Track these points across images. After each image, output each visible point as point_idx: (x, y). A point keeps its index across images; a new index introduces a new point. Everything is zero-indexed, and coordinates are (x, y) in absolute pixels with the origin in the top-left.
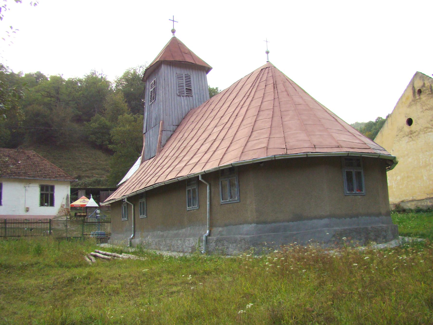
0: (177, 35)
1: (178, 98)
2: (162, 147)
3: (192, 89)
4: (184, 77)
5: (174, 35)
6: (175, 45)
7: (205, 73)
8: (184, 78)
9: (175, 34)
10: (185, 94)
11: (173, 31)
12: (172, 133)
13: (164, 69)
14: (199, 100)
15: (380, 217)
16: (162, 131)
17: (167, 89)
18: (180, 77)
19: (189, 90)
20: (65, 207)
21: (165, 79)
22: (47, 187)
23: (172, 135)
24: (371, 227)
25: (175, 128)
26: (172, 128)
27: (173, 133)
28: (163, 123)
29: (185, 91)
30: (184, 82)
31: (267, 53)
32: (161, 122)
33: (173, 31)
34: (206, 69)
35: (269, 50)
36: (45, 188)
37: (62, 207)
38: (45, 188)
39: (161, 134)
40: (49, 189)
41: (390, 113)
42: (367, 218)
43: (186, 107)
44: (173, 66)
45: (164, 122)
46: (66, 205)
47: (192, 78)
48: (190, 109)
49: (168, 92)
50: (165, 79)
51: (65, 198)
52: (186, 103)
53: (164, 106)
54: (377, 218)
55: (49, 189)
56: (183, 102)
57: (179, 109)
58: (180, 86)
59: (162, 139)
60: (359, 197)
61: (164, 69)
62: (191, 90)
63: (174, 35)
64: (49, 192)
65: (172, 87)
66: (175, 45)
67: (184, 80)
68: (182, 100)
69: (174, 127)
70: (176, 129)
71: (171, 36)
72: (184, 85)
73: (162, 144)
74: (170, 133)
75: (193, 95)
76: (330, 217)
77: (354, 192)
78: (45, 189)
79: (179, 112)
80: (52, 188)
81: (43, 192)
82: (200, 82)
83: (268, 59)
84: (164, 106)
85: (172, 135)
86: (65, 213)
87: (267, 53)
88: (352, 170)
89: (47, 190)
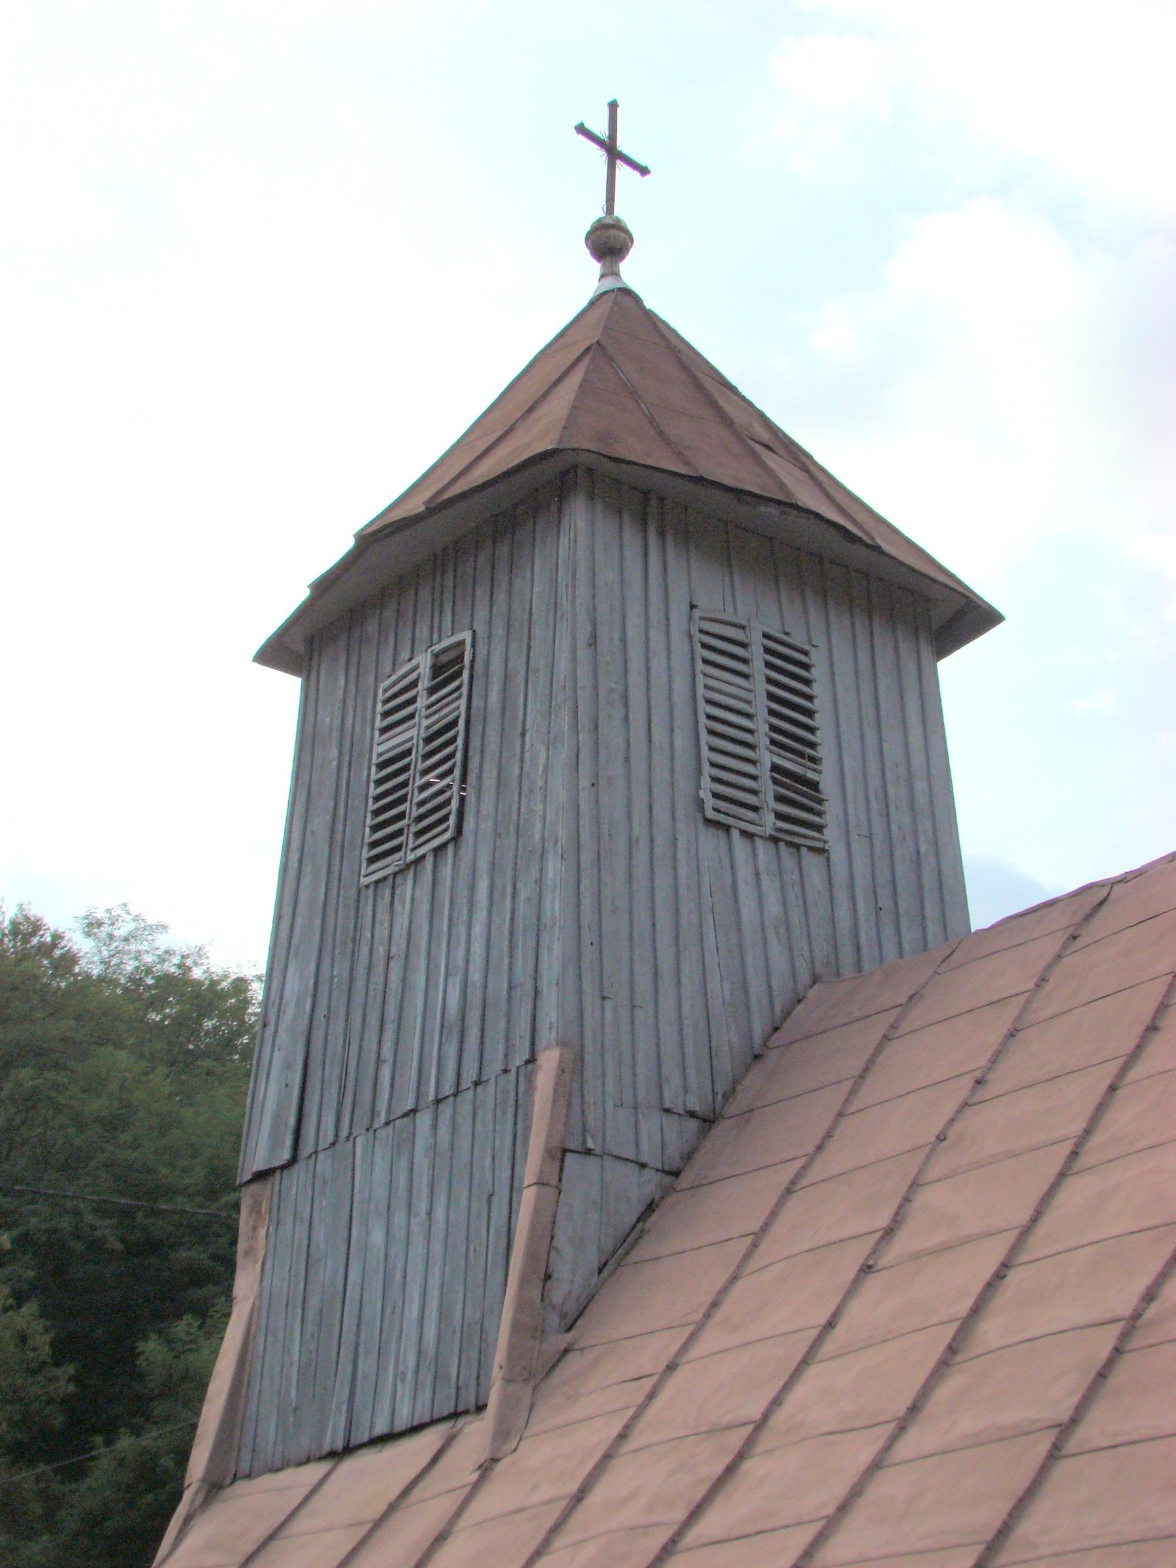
0: (633, 272)
1: (709, 841)
2: (554, 1320)
3: (827, 781)
4: (757, 657)
5: (610, 272)
6: (619, 344)
7: (926, 651)
8: (758, 668)
10: (769, 831)
11: (609, 243)
12: (650, 1183)
13: (583, 535)
14: (885, 902)
16: (559, 1154)
17: (613, 736)
18: (721, 650)
19: (800, 792)
21: (593, 642)
23: (650, 1208)
25: (678, 1134)
26: (657, 1137)
27: (667, 1191)
28: (574, 1071)
29: (768, 789)
30: (761, 705)
32: (549, 1060)
33: (609, 243)
34: (958, 616)
39: (553, 1184)
43: (777, 951)
44: (823, 594)
45: (581, 1059)
47: (818, 673)
48: (804, 977)
49: (619, 770)
50: (593, 642)
52: (773, 907)
53: (587, 902)
56: (746, 892)
57: (712, 959)
58: (726, 730)
59: (561, 1241)
61: (583, 535)
62: (814, 786)
63: (610, 272)
65: (659, 735)
66: (619, 344)
67: (761, 687)
68: (744, 872)
69: (670, 1122)
70: (688, 1157)
71: (584, 279)
72: (761, 725)
73: (559, 1293)
74: (636, 1188)
75: (832, 836)
76: (812, 957)
79: (713, 985)
82: (891, 730)
84: (587, 902)
85: (650, 1208)
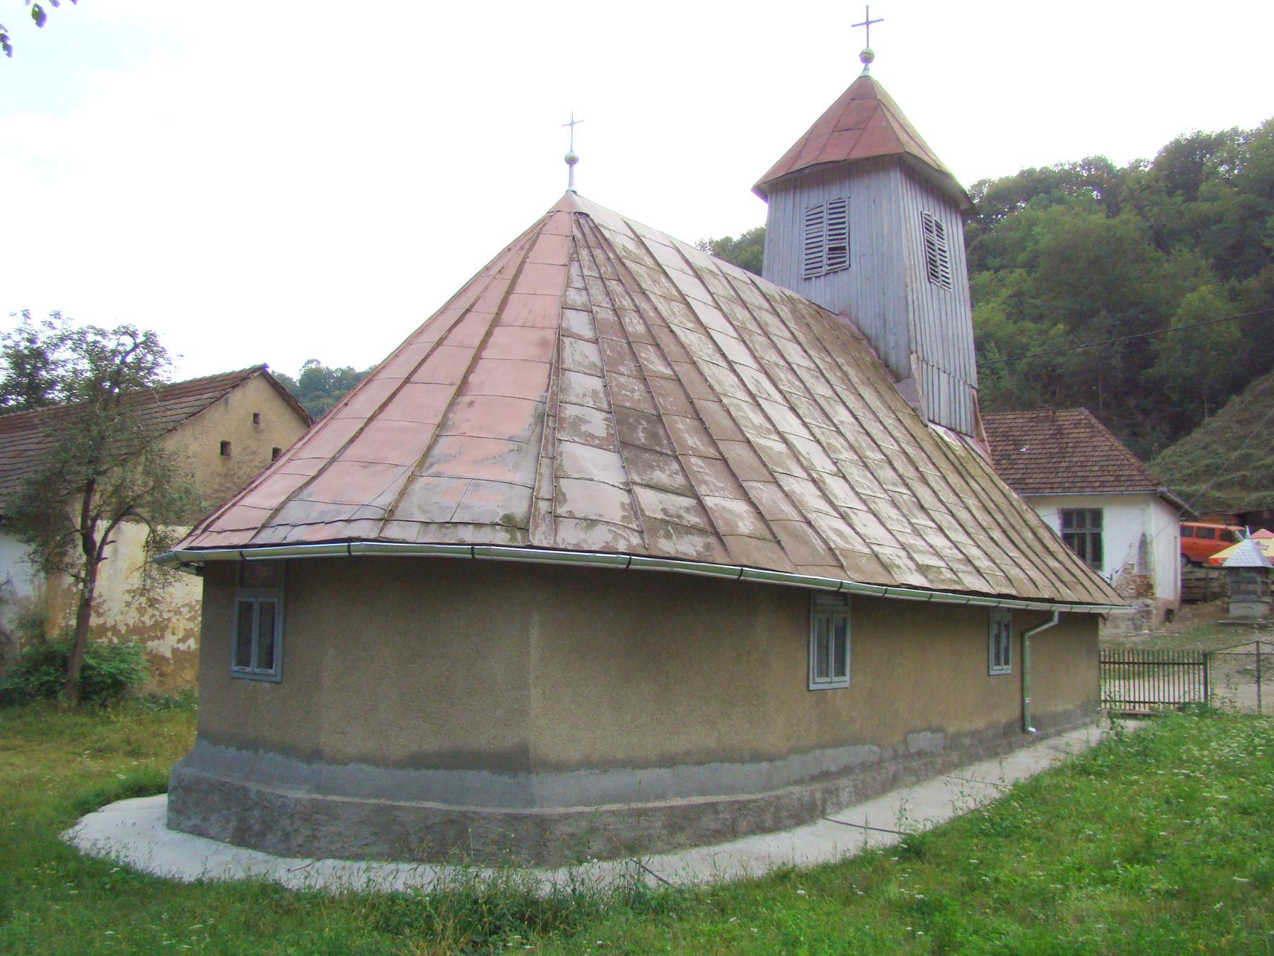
6: (863, 106)
9: (871, 66)
11: (867, 58)
15: (315, 766)
18: (813, 218)
20: (1135, 571)
22: (1081, 514)
24: (258, 791)
31: (571, 161)
33: (867, 58)
35: (577, 154)
36: (1075, 517)
37: (1126, 570)
38: (1075, 517)
40: (1088, 521)
41: (360, 368)
42: (280, 758)
46: (1140, 564)
51: (1137, 544)
54: (303, 767)
55: (1088, 521)
60: (267, 686)
64: (1088, 530)
66: (863, 106)
77: (248, 669)
78: (1075, 522)
80: (1097, 516)
81: (1069, 531)
83: (571, 184)
86: (1137, 589)
87: (571, 161)
88: (252, 600)
89: (1082, 524)
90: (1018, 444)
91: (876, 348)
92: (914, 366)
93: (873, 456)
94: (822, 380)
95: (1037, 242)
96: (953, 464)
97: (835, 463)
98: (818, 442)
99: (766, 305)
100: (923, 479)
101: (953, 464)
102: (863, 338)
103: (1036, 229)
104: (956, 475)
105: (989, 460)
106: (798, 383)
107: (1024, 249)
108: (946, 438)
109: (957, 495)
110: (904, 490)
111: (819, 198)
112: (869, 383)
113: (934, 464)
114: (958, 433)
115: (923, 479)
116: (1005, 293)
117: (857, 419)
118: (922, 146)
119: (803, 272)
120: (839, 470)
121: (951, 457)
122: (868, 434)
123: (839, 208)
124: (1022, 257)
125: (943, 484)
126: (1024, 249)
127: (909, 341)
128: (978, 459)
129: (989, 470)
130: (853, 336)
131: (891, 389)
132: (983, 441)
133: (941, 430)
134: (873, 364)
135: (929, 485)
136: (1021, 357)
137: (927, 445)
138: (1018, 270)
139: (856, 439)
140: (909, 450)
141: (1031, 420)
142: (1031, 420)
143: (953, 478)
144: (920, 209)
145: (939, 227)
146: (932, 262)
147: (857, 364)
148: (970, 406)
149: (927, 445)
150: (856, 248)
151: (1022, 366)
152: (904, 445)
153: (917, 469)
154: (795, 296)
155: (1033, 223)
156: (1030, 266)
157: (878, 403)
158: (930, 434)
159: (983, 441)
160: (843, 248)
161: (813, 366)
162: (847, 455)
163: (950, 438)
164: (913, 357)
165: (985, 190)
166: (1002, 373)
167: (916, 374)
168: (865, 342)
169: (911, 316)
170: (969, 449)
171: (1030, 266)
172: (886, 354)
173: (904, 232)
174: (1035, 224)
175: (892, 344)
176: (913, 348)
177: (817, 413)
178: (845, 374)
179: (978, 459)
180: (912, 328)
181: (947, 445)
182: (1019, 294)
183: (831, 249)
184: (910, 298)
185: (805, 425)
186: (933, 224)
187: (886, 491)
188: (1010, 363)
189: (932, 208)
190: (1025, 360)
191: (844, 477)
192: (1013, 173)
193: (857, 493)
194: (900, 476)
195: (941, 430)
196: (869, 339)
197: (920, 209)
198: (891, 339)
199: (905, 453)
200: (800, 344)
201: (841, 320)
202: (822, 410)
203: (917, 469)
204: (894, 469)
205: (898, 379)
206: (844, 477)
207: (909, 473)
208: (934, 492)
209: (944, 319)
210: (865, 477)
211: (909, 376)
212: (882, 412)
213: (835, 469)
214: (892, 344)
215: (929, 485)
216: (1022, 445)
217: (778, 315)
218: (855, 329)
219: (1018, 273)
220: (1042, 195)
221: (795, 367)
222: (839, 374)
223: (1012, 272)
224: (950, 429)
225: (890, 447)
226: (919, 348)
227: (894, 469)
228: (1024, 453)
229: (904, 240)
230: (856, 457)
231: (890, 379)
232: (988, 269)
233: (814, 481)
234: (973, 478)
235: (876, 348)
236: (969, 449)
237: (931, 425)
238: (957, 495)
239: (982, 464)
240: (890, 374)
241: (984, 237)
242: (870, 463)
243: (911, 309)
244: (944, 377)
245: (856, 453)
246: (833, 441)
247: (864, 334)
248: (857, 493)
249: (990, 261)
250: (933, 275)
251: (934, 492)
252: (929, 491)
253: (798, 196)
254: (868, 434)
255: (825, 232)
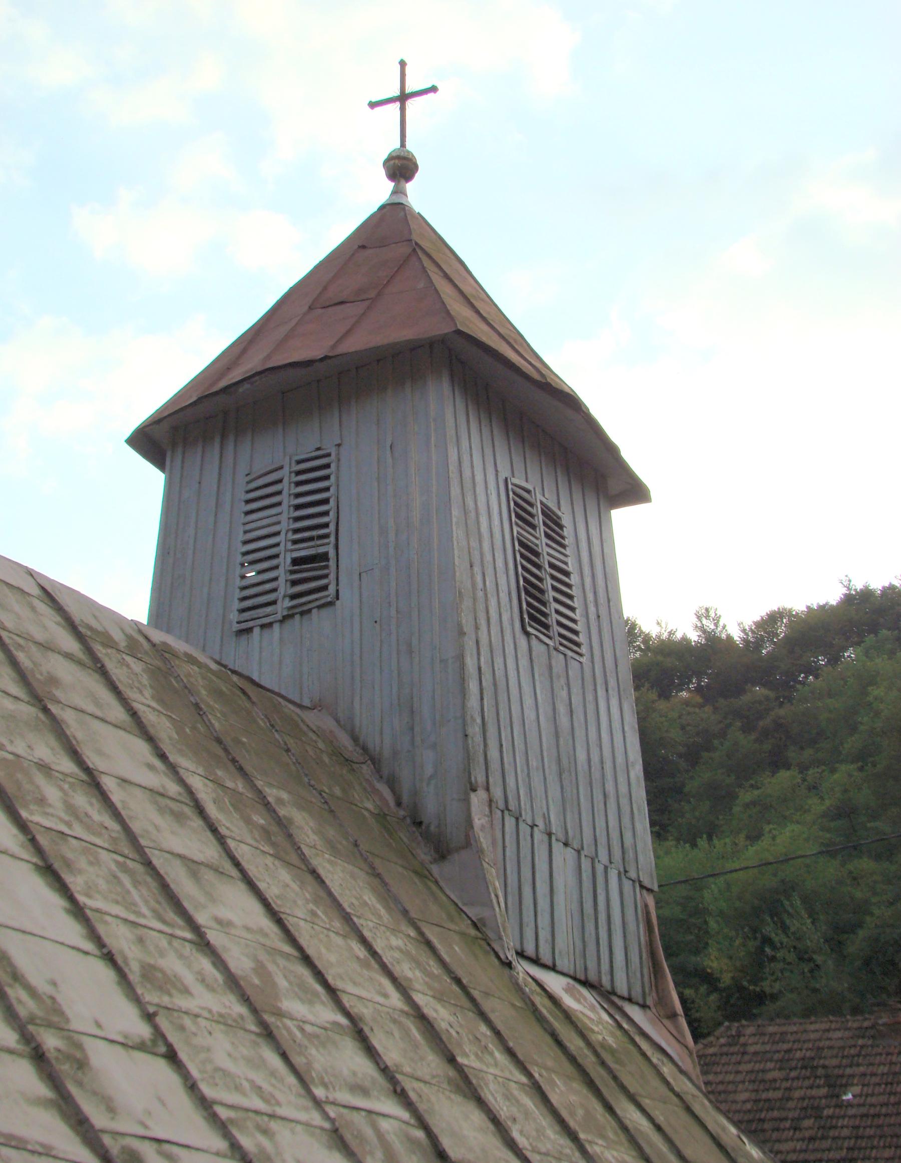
11: (401, 168)
33: (401, 168)
90: (836, 1085)
91: (392, 783)
92: (479, 821)
93: (307, 1011)
94: (197, 823)
95: (877, 714)
96: (572, 1059)
97: (150, 1018)
98: (110, 958)
99: (71, 645)
100: (467, 1087)
101: (572, 1059)
102: (365, 759)
103: (876, 692)
104: (578, 1086)
105: (687, 1064)
106: (99, 815)
107: (853, 729)
108: (569, 1001)
109: (573, 1136)
110: (390, 1106)
111: (273, 454)
112: (356, 853)
113: (511, 1053)
114: (609, 997)
115: (467, 1087)
116: (817, 806)
117: (279, 921)
118: (516, 340)
119: (234, 616)
120: (159, 1034)
121: (574, 1043)
122: (307, 960)
123: (315, 472)
124: (851, 744)
125: (528, 1102)
126: (853, 729)
127: (468, 758)
128: (655, 1058)
129: (683, 1085)
130: (337, 753)
131: (423, 874)
132: (673, 1016)
133: (555, 983)
134: (381, 817)
135: (481, 1102)
136: (853, 928)
137: (501, 1010)
138: (843, 768)
139: (260, 969)
140: (442, 1015)
141: (862, 1032)
142: (862, 1032)
143: (567, 1093)
144: (504, 473)
145: (553, 521)
146: (531, 590)
147: (329, 810)
148: (637, 931)
149: (501, 1010)
150: (354, 550)
151: (857, 944)
152: (419, 998)
153: (451, 1060)
154: (179, 645)
155: (868, 680)
156: (862, 757)
157: (369, 898)
158: (518, 989)
159: (673, 1016)
160: (324, 557)
161: (173, 788)
162: (206, 998)
163: (583, 1005)
164: (477, 800)
165: (782, 631)
166: (819, 959)
167: (484, 840)
168: (366, 770)
169: (473, 702)
170: (632, 1034)
171: (862, 757)
172: (415, 793)
173: (456, 512)
174: (872, 682)
175: (429, 770)
176: (479, 777)
177: (143, 897)
178: (283, 824)
179: (655, 1058)
180: (475, 730)
181: (567, 1016)
182: (845, 812)
183: (295, 561)
184: (470, 663)
185: (78, 911)
186: (537, 510)
187: (318, 1104)
188: (836, 945)
189: (535, 477)
190: (861, 933)
191: (172, 1056)
192: (833, 596)
193: (205, 1104)
194: (385, 1070)
195: (555, 983)
196: (375, 761)
197: (504, 473)
198: (428, 758)
199: (421, 1018)
200: (150, 739)
201: (311, 718)
202: (164, 886)
203: (451, 1060)
204: (370, 1051)
205: (442, 853)
206: (172, 1056)
207: (421, 1066)
208: (495, 1120)
209: (564, 721)
210: (259, 1064)
211: (468, 842)
212: (374, 915)
213: (144, 1031)
214: (429, 770)
215: (481, 1102)
216: (845, 1087)
217: (103, 672)
218: (344, 740)
219: (845, 772)
220: (884, 632)
221: (109, 783)
222: (259, 819)
223: (833, 771)
224: (585, 983)
225: (371, 996)
226: (495, 780)
227: (370, 1051)
228: (849, 1105)
229: (458, 533)
230: (239, 1009)
231: (424, 854)
232: (788, 767)
233: (39, 1057)
234: (633, 1099)
235: (392, 783)
236: (632, 1034)
237: (523, 968)
238: (573, 1136)
239: (667, 1070)
240: (415, 831)
241: (782, 712)
242: (286, 1029)
243: (473, 686)
244: (563, 857)
245: (246, 999)
246: (172, 964)
247: (365, 749)
248: (205, 1104)
249: (792, 754)
250: (534, 617)
251: (495, 1120)
252: (477, 1117)
253: (230, 448)
254: (307, 960)
255: (285, 525)
